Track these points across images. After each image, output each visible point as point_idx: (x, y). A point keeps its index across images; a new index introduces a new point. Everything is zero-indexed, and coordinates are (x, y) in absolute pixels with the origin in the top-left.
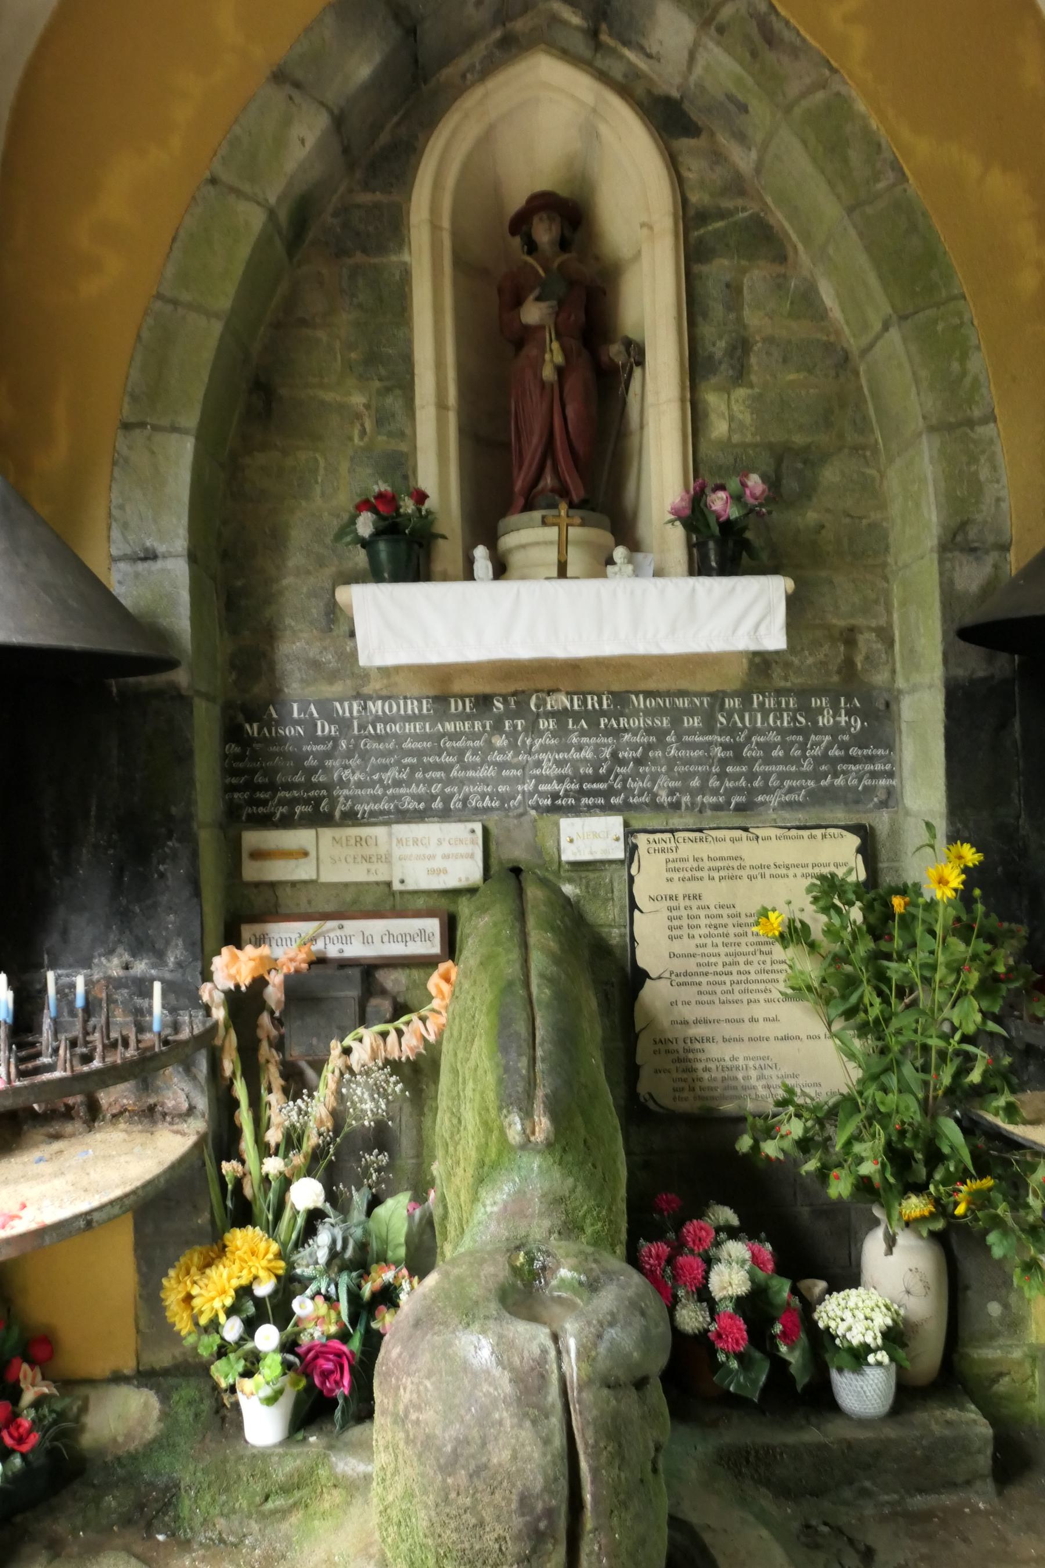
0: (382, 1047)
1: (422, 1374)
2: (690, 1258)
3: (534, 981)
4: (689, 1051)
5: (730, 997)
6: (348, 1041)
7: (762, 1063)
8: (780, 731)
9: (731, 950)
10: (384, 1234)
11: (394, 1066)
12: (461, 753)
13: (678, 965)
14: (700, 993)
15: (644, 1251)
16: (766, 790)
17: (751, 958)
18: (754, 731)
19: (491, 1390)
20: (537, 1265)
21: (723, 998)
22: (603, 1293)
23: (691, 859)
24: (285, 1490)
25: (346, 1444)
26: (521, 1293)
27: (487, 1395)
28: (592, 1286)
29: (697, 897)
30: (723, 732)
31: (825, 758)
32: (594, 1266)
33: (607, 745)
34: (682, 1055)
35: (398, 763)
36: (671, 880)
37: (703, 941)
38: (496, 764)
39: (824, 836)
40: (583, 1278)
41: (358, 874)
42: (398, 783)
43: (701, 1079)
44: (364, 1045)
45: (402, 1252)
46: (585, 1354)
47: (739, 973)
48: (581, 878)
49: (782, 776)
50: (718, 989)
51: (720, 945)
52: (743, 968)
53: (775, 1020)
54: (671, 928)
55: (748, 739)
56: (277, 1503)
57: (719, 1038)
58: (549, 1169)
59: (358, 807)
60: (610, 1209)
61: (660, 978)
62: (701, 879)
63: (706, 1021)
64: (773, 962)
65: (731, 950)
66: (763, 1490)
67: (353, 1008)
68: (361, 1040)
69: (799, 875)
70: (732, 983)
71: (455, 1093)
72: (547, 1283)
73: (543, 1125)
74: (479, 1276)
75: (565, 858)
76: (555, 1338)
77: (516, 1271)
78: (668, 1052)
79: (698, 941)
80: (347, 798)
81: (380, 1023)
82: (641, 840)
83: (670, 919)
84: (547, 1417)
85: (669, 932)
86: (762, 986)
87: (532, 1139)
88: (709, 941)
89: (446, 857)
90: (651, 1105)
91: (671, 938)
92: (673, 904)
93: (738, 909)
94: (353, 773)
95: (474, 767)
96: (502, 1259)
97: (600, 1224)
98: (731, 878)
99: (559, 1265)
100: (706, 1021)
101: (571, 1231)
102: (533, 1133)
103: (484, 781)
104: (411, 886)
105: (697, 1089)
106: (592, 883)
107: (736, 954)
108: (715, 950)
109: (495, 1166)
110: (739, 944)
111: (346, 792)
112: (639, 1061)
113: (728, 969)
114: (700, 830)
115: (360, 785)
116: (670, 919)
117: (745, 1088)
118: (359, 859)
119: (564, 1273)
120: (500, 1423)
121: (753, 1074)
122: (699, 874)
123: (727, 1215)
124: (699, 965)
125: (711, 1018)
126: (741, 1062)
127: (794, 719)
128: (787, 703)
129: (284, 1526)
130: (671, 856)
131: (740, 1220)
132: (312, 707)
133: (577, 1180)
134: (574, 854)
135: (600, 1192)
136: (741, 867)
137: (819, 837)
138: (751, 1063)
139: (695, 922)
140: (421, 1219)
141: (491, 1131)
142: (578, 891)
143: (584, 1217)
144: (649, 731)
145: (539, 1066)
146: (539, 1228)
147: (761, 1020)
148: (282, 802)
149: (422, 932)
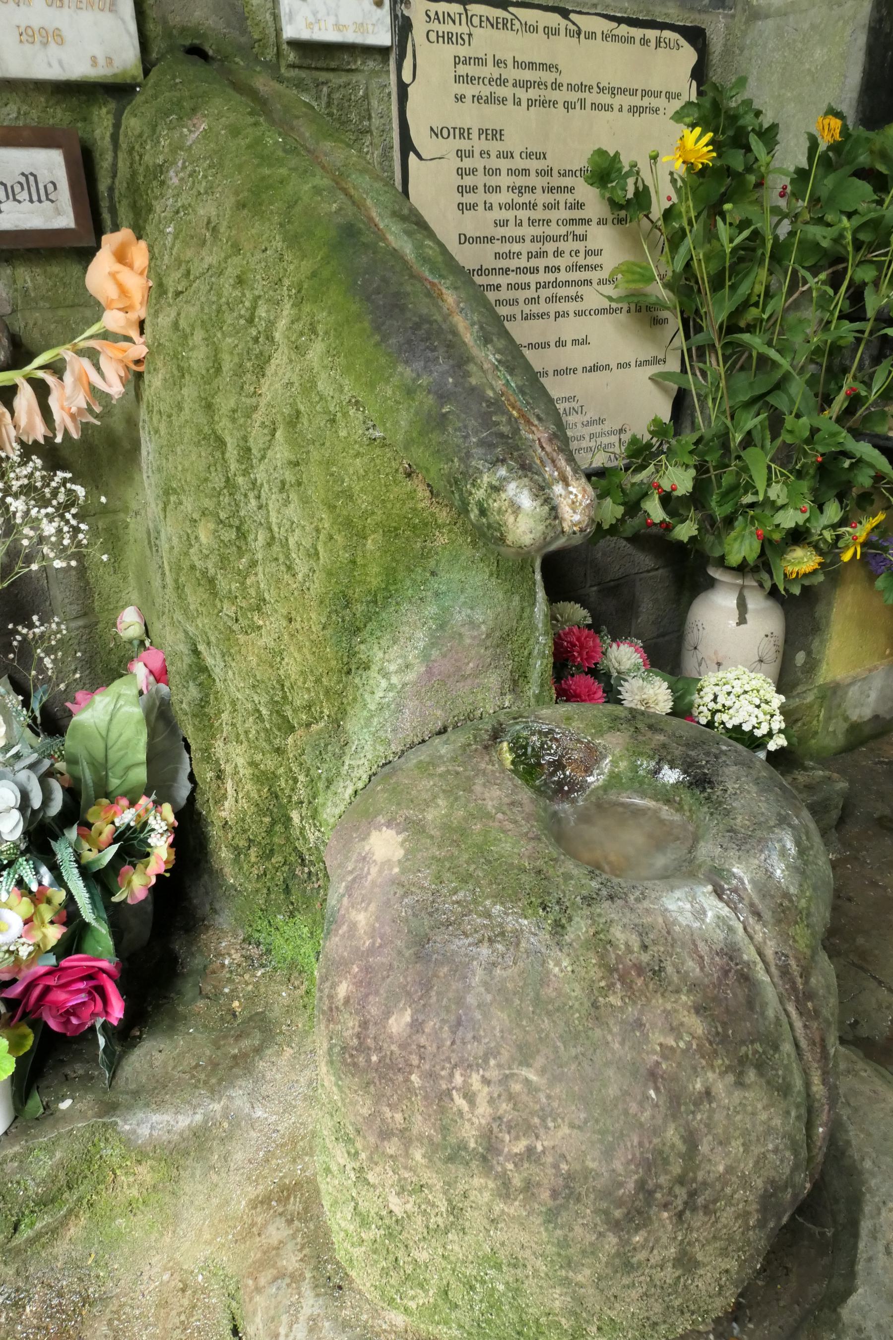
1: (505, 1056)
5: (535, 309)
9: (538, 231)
17: (562, 245)
21: (527, 310)
24: (45, 1202)
25: (136, 1094)
27: (667, 1052)
29: (497, 134)
36: (460, 98)
47: (547, 269)
48: (318, 85)
50: (521, 295)
52: (551, 261)
53: (585, 342)
54: (461, 190)
56: (38, 1226)
62: (504, 101)
64: (587, 253)
65: (538, 231)
70: (539, 286)
71: (217, 481)
75: (290, 32)
84: (776, 1048)
85: (458, 198)
86: (571, 291)
88: (509, 215)
91: (461, 207)
92: (464, 145)
98: (543, 103)
106: (337, 96)
107: (545, 239)
108: (519, 232)
109: (382, 598)
113: (534, 263)
116: (461, 172)
120: (708, 1093)
122: (501, 92)
124: (497, 256)
129: (61, 1248)
130: (463, 51)
134: (310, 26)
136: (556, 86)
147: (569, 343)
149: (29, 178)
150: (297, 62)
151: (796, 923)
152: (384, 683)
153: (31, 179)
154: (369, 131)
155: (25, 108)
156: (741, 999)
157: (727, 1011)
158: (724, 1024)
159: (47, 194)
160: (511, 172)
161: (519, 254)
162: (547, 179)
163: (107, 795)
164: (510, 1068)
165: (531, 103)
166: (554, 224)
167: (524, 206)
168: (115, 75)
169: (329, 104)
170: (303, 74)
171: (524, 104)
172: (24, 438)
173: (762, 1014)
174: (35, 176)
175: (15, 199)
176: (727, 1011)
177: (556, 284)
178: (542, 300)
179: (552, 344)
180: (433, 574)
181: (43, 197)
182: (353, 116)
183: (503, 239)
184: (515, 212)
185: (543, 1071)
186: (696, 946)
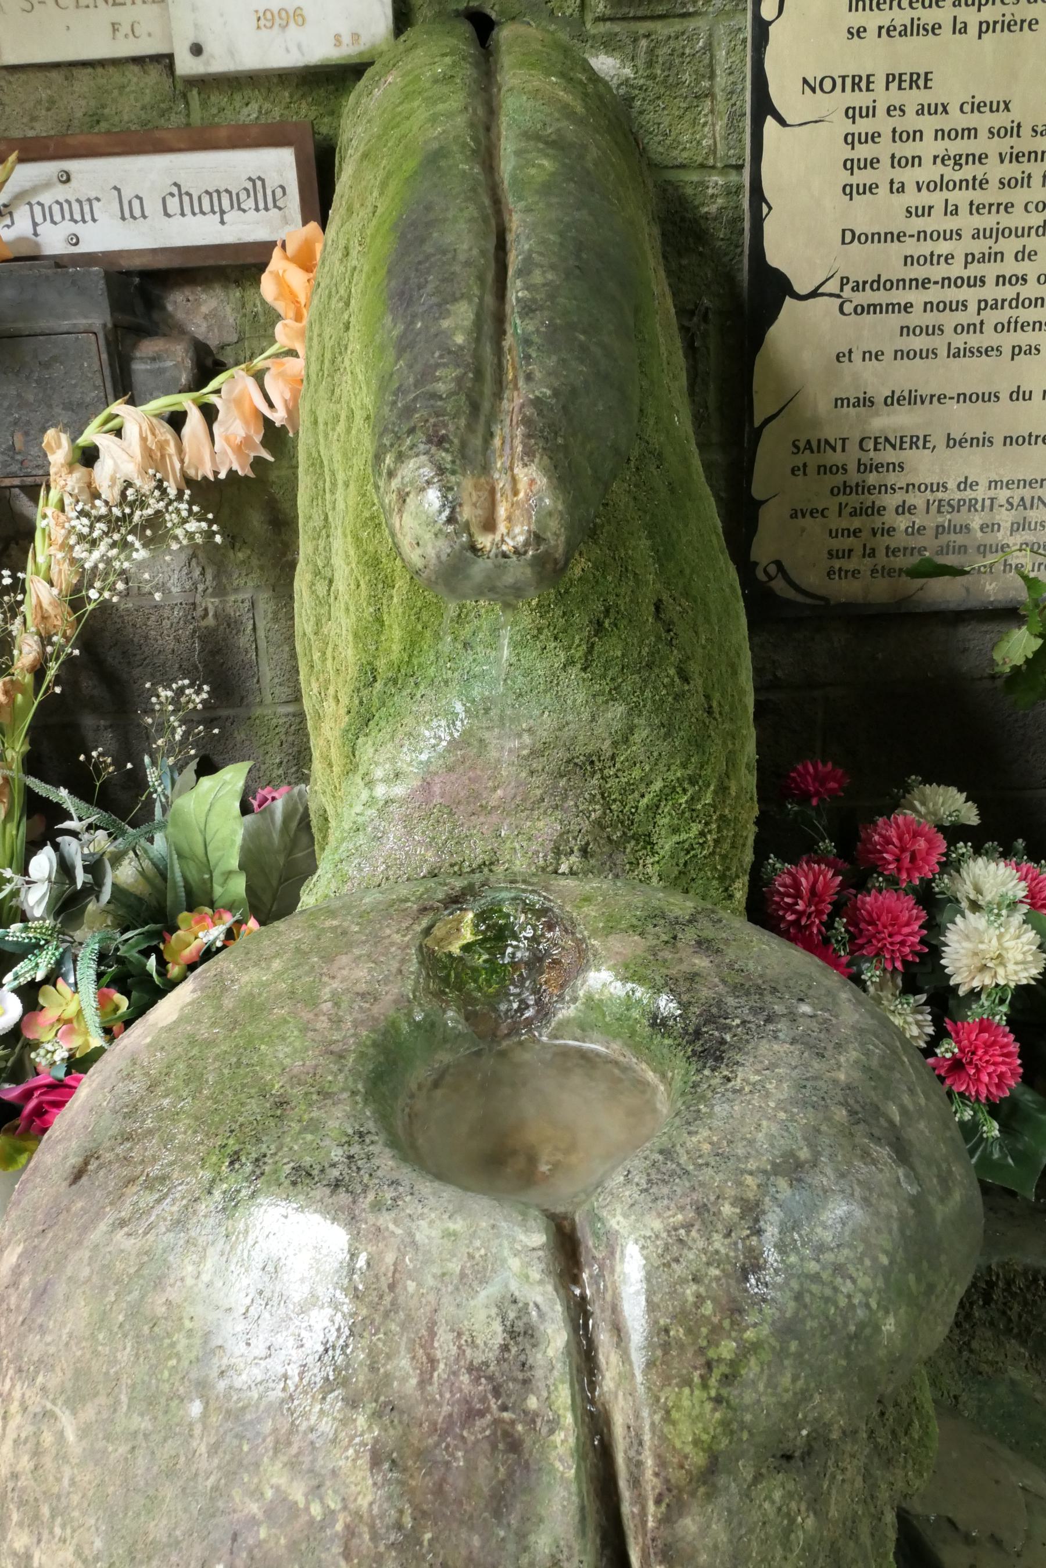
0: (172, 449)
1: (53, 1380)
2: (888, 898)
3: (508, 147)
4: (863, 467)
5: (974, 340)
6: (92, 435)
7: (1027, 493)
9: (987, 221)
10: (199, 850)
11: (207, 493)
13: (861, 263)
14: (905, 330)
15: (781, 883)
19: (298, 1493)
20: (517, 950)
21: (958, 342)
22: (746, 1074)
26: (447, 1086)
27: (282, 1510)
28: (705, 1043)
29: (919, 80)
32: (701, 963)
34: (853, 477)
36: (856, 33)
37: (925, 198)
40: (667, 1005)
43: (890, 531)
44: (126, 443)
45: (239, 886)
46: (686, 1343)
50: (950, 320)
51: (964, 209)
52: (1010, 267)
54: (849, 165)
57: (938, 439)
58: (552, 681)
60: (722, 789)
61: (814, 294)
63: (913, 399)
65: (987, 221)
66: (1013, 1346)
67: (93, 359)
68: (118, 432)
70: (983, 305)
72: (544, 1012)
73: (523, 499)
74: (312, 1001)
76: (568, 1252)
77: (443, 973)
78: (823, 469)
79: (912, 198)
81: (167, 393)
83: (850, 140)
85: (845, 177)
87: (485, 541)
88: (936, 199)
90: (779, 586)
91: (849, 191)
92: (861, 99)
93: (1016, 114)
96: (401, 938)
97: (696, 828)
99: (583, 959)
100: (913, 399)
101: (616, 846)
102: (489, 525)
104: (219, 61)
105: (881, 552)
106: (663, 51)
107: (999, 233)
108: (951, 223)
109: (404, 676)
110: (1008, 207)
112: (758, 491)
113: (975, 270)
116: (850, 140)
117: (983, 550)
119: (601, 981)
121: (1005, 517)
123: (953, 804)
124: (908, 260)
125: (924, 391)
126: (981, 493)
131: (981, 815)
133: (634, 710)
135: (698, 743)
138: (1003, 495)
139: (909, 149)
140: (287, 818)
141: (388, 583)
142: (628, 72)
143: (654, 808)
145: (517, 325)
146: (522, 843)
149: (257, 182)
150: (608, 12)
151: (688, 1382)
152: (365, 795)
153: (259, 183)
154: (710, 94)
155: (267, 106)
156: (483, 1481)
157: (439, 1491)
158: (421, 1515)
159: (275, 201)
160: (940, 134)
161: (948, 258)
162: (1009, 141)
163: (211, 904)
164: (54, 1402)
165: (985, 27)
166: (1019, 208)
167: (963, 184)
168: (361, 54)
169: (650, 64)
170: (616, 27)
171: (973, 30)
172: (191, 472)
173: (521, 1536)
174: (263, 181)
175: (240, 209)
176: (439, 1491)
177: (1017, 302)
178: (988, 328)
179: (1004, 396)
180: (466, 645)
181: (270, 204)
182: (686, 77)
183: (921, 235)
184: (946, 194)
185: (84, 1432)
186: (432, 1334)
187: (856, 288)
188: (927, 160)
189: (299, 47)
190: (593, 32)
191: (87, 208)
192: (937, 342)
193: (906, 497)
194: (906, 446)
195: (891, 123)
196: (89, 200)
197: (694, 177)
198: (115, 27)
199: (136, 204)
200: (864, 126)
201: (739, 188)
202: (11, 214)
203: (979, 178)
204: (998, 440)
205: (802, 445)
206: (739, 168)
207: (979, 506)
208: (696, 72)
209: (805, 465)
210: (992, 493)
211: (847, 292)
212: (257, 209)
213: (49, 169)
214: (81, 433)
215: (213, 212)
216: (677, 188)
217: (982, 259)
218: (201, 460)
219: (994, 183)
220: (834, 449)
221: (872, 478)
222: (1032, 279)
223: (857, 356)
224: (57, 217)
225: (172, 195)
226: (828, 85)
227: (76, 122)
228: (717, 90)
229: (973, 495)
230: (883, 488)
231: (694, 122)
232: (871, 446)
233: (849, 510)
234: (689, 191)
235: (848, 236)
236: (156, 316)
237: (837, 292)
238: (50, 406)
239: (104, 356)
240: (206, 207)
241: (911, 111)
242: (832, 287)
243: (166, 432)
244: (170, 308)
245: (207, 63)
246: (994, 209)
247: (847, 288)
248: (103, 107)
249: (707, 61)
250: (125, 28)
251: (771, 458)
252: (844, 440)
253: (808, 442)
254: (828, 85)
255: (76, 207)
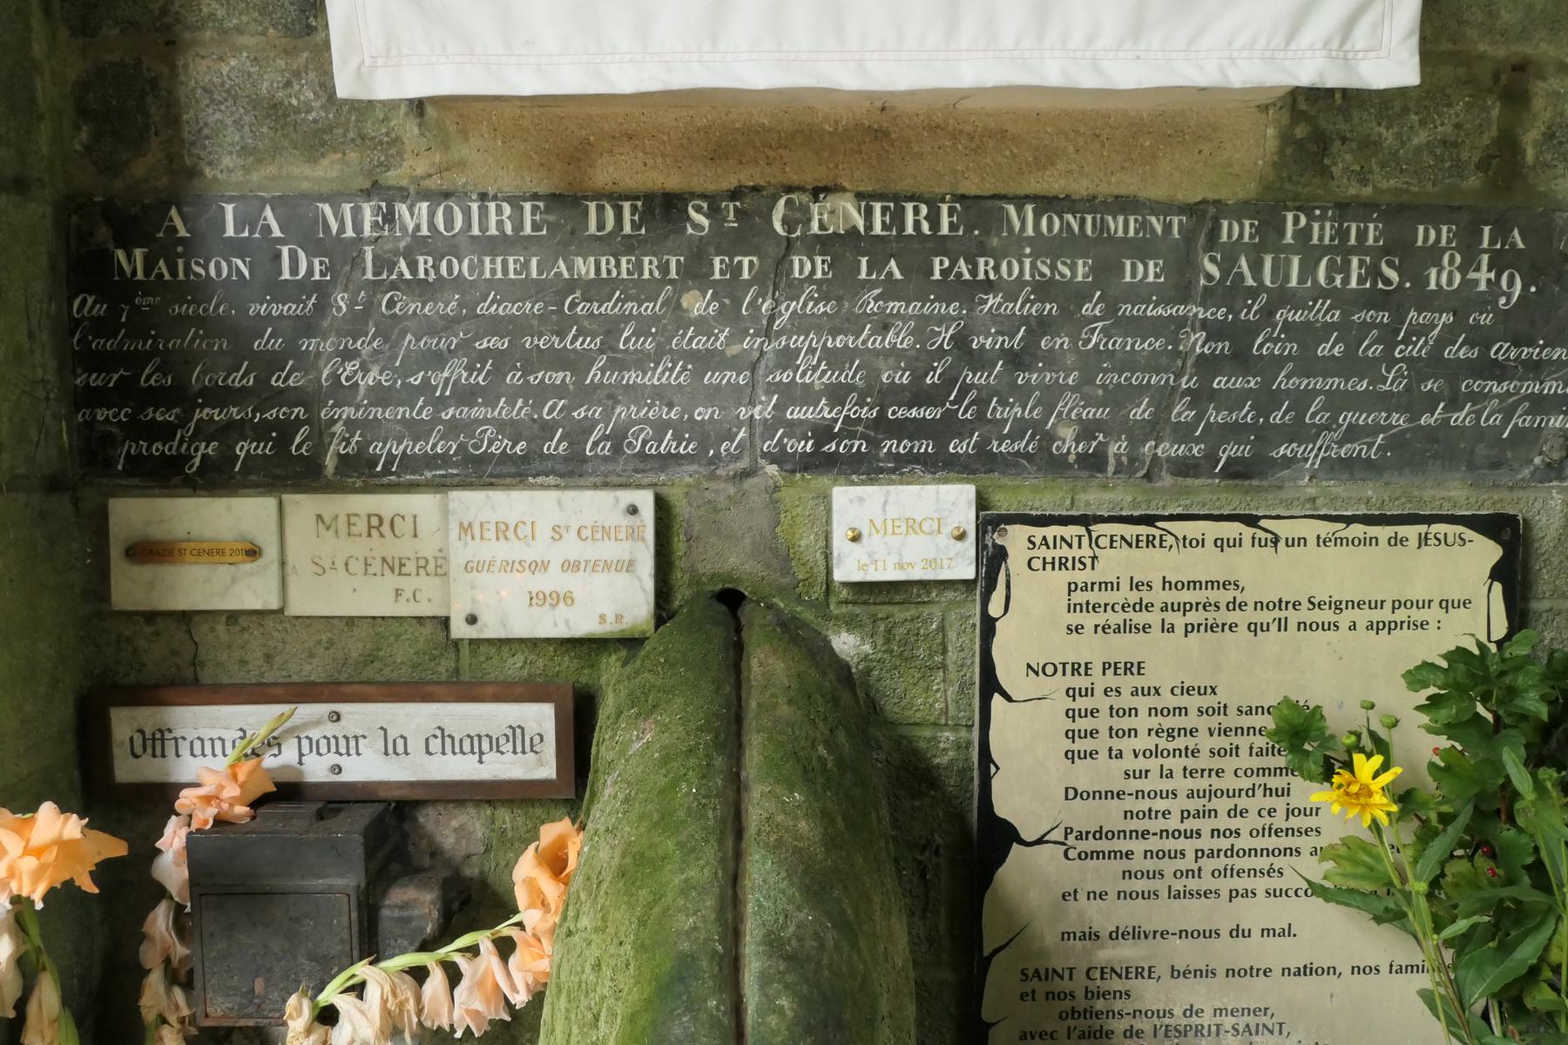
5: (1193, 884)
7: (1252, 1020)
8: (1340, 298)
9: (1202, 783)
12: (610, 328)
13: (1084, 815)
14: (1127, 874)
16: (1299, 432)
18: (1282, 297)
21: (1178, 885)
23: (1125, 585)
30: (1209, 296)
31: (1435, 363)
33: (942, 320)
34: (1081, 1004)
35: (466, 345)
37: (1141, 763)
38: (691, 356)
39: (1423, 540)
41: (374, 598)
42: (466, 396)
49: (1337, 403)
50: (1169, 866)
51: (1178, 773)
52: (1223, 822)
54: (1071, 735)
55: (1268, 313)
57: (1163, 970)
59: (376, 448)
61: (1040, 841)
63: (1136, 934)
65: (1202, 783)
67: (345, 917)
69: (1361, 626)
70: (1199, 854)
78: (1050, 996)
79: (1129, 763)
80: (351, 424)
82: (1016, 538)
86: (1262, 863)
88: (1153, 764)
89: (571, 566)
92: (1080, 682)
93: (1222, 697)
94: (365, 369)
95: (641, 361)
100: (1136, 934)
103: (662, 395)
107: (1212, 794)
108: (1166, 785)
111: (348, 412)
112: (987, 1014)
113: (1191, 824)
114: (1149, 520)
115: (381, 396)
116: (1071, 714)
118: (376, 566)
122: (1140, 618)
125: (1148, 928)
126: (1206, 1019)
127: (1374, 272)
128: (1362, 235)
132: (268, 212)
134: (863, 567)
136: (1235, 605)
137: (1413, 541)
138: (1228, 1022)
139: (1126, 723)
142: (867, 648)
144: (1044, 289)
147: (1256, 933)
148: (204, 432)
149: (517, 731)
153: (518, 731)
154: (944, 667)
159: (532, 746)
161: (1166, 814)
165: (1189, 629)
166: (1229, 773)
167: (1177, 752)
170: (858, 610)
171: (1180, 630)
172: (428, 1024)
177: (1231, 852)
178: (1206, 873)
179: (1225, 933)
181: (528, 748)
183: (1139, 794)
184: (1160, 761)
187: (1079, 837)
188: (1143, 732)
189: (567, 622)
190: (836, 612)
191: (352, 743)
192: (1157, 885)
193: (1133, 1022)
194: (1143, 544)
195: (1108, 702)
196: (356, 738)
197: (927, 733)
198: (398, 593)
199: (400, 742)
200: (1083, 703)
201: (969, 744)
202: (279, 745)
203: (1191, 747)
204: (1221, 972)
205: (1030, 973)
206: (969, 727)
207: (1205, 1032)
208: (930, 648)
209: (1033, 992)
210: (1218, 1020)
211: (1071, 840)
212: (515, 752)
213: (322, 709)
214: (322, 990)
215: (473, 752)
216: (910, 742)
217: (1197, 815)
218: (439, 1015)
219: (1205, 752)
220: (1062, 977)
221: (1100, 1005)
222: (1245, 833)
223: (1082, 896)
224: (323, 750)
225: (435, 736)
226: (1050, 669)
227: (351, 661)
228: (948, 662)
229: (1199, 1021)
230: (1111, 1013)
231: (927, 689)
232: (1098, 975)
233: (1077, 1033)
234: (922, 745)
235: (1071, 794)
236: (407, 826)
237: (1062, 839)
238: (295, 958)
239: (354, 915)
240: (467, 748)
241: (1126, 692)
242: (1057, 835)
243: (406, 987)
244: (421, 820)
245: (481, 630)
246: (1206, 774)
247: (1071, 837)
248: (378, 649)
249: (939, 641)
250: (408, 594)
251: (1000, 985)
252: (1071, 970)
253: (1037, 971)
254: (1050, 669)
255: (342, 742)
